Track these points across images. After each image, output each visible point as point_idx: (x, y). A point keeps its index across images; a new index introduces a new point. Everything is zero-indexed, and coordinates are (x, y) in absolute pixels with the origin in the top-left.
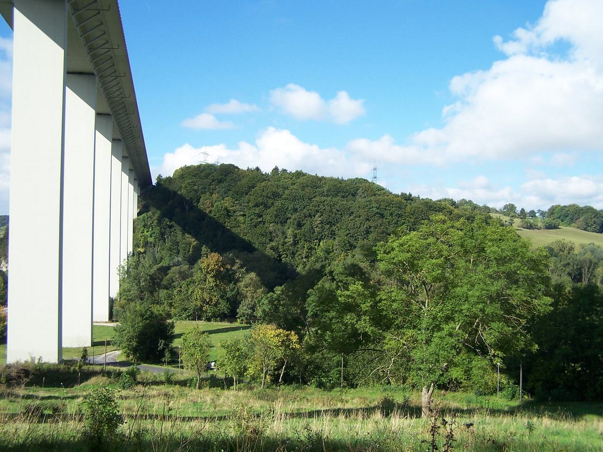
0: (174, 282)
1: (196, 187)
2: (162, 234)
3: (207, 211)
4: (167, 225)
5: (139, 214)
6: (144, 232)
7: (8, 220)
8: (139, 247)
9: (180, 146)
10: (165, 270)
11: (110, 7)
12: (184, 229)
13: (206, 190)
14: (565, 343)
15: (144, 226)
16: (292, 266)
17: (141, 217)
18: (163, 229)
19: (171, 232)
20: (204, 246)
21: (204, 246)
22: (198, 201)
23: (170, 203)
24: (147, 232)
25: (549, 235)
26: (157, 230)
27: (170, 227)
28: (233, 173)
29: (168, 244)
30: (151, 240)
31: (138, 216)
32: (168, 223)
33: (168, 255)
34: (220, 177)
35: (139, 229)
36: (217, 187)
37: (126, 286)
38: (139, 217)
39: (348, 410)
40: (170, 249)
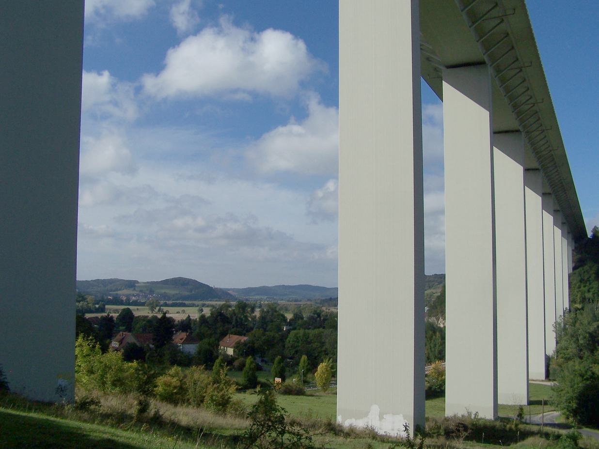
8: (575, 303)
11: (514, 9)
15: (581, 281)
35: (576, 285)
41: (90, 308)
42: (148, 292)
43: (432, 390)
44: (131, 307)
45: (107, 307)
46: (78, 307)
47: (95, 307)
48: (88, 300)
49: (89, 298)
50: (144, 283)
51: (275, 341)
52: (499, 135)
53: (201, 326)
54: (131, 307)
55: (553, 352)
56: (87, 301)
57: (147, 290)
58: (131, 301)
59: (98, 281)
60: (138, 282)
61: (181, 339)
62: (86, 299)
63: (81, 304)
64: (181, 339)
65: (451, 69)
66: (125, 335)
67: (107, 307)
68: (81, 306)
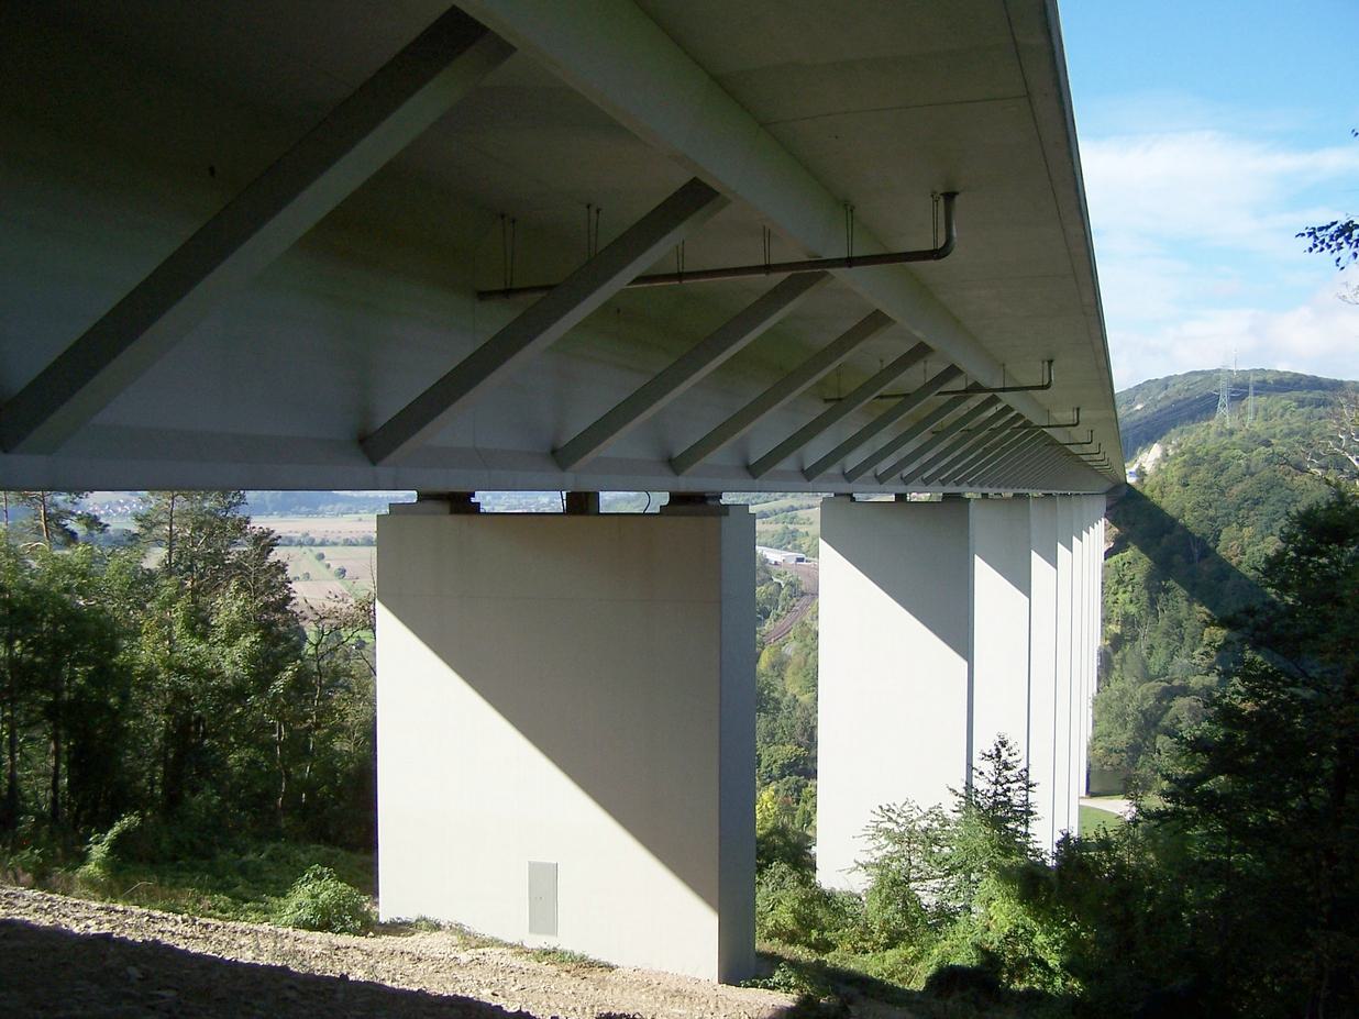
0: (1181, 722)
1: (1211, 512)
2: (1153, 602)
3: (1234, 562)
7: (457, 8)
12: (1192, 595)
13: (1232, 519)
14: (1051, 983)
19: (1168, 600)
20: (1290, 803)
21: (1290, 803)
22: (1217, 539)
23: (1164, 541)
24: (1125, 592)
28: (1281, 487)
29: (1163, 623)
31: (1105, 559)
33: (1163, 645)
34: (1258, 495)
36: (1252, 513)
37: (1104, 726)
40: (1167, 634)
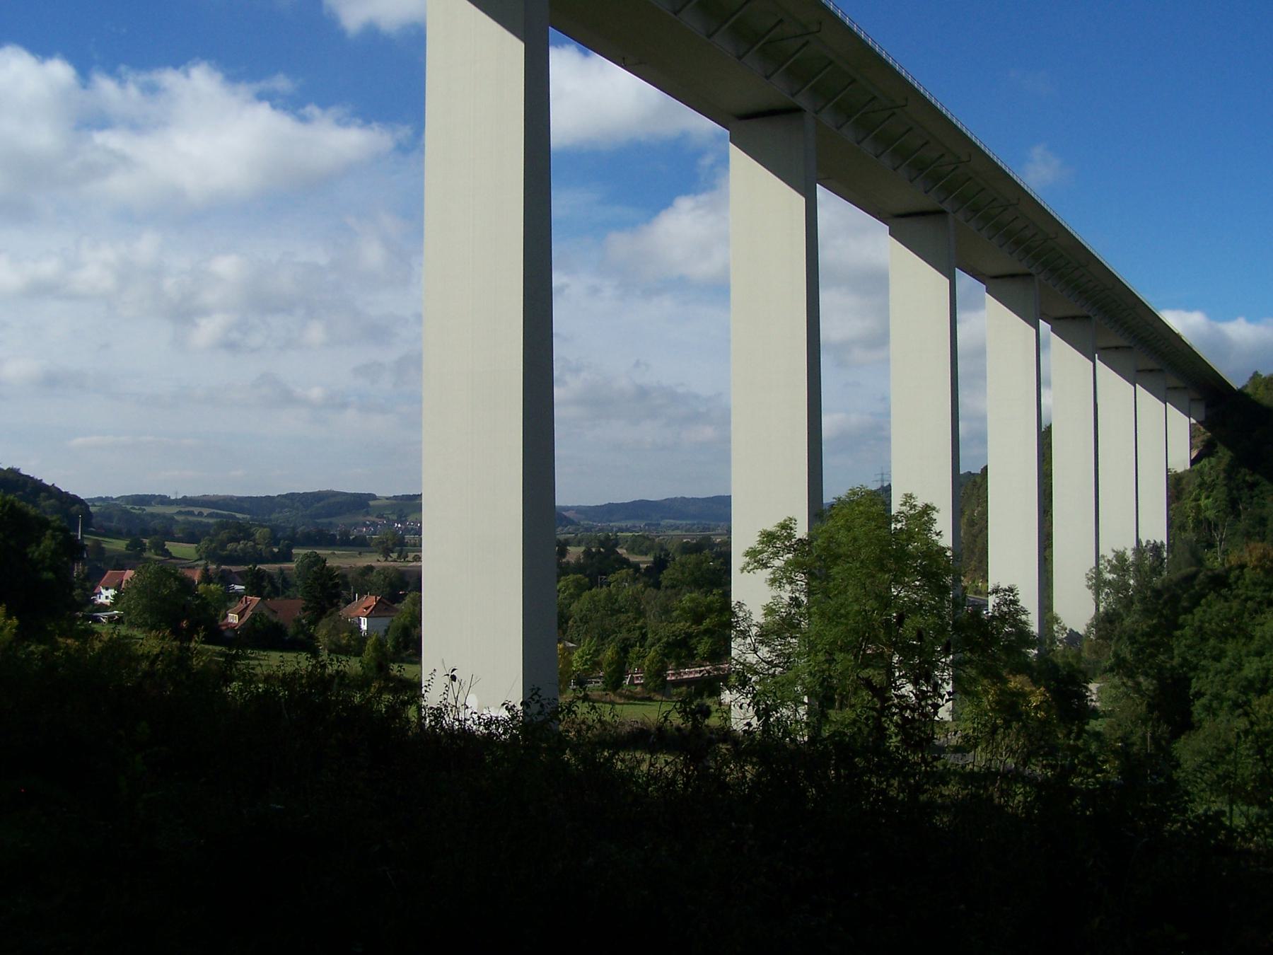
4: (1244, 481)
5: (1193, 462)
6: (1199, 500)
8: (1185, 530)
9: (1181, 473)
10: (1227, 550)
11: (820, 23)
15: (1200, 486)
16: (787, 733)
17: (1197, 466)
18: (1234, 492)
19: (1252, 497)
25: (651, 703)
26: (1221, 492)
27: (1252, 486)
30: (1210, 514)
31: (1191, 465)
32: (1247, 478)
35: (1191, 493)
38: (1194, 467)
39: (692, 656)
41: (261, 554)
42: (395, 518)
43: (174, 636)
44: (321, 552)
45: (294, 551)
46: (236, 551)
47: (272, 551)
48: (257, 535)
49: (259, 533)
50: (387, 499)
51: (716, 614)
52: (903, 220)
53: (176, 579)
54: (321, 552)
55: (1085, 627)
56: (254, 541)
57: (393, 513)
58: (351, 538)
59: (291, 497)
60: (372, 497)
61: (367, 609)
62: (253, 535)
63: (241, 546)
64: (367, 609)
65: (747, 121)
66: (251, 601)
67: (294, 551)
68: (241, 549)
